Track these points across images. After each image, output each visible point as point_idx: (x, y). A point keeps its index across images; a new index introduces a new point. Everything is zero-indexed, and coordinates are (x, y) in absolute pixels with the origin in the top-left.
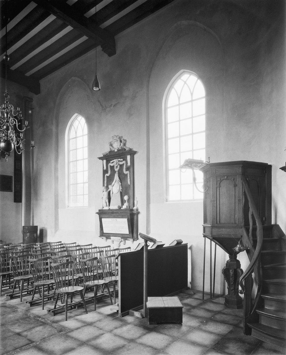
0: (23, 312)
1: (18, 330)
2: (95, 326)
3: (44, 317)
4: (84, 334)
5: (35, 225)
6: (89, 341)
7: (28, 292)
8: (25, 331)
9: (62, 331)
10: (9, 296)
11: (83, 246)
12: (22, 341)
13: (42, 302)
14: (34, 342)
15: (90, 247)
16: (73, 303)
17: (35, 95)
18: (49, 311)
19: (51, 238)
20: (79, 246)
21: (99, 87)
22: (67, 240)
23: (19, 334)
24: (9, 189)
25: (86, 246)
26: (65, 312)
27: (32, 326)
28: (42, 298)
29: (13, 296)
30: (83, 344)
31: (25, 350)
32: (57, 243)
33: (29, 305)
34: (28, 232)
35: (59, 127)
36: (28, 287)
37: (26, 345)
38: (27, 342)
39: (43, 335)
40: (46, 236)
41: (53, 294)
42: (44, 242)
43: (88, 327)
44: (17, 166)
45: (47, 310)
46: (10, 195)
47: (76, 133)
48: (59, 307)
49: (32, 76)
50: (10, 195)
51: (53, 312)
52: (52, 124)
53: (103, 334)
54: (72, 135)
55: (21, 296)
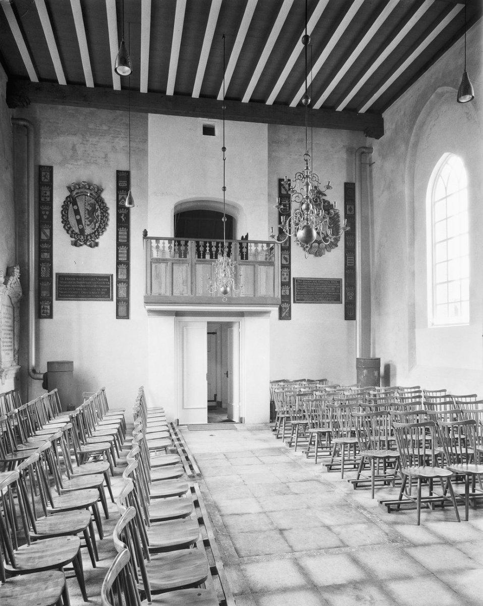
0: (342, 495)
1: (328, 521)
2: (460, 550)
3: (371, 510)
4: (433, 559)
5: (377, 357)
6: (441, 572)
7: (355, 465)
8: (338, 525)
9: (397, 542)
10: (326, 465)
11: (455, 397)
12: (332, 541)
13: (370, 486)
14: (348, 546)
15: (473, 399)
16: (433, 496)
17: (376, 141)
18: (381, 502)
19: (402, 380)
20: (449, 396)
21: (470, 94)
22: (430, 384)
23: (329, 528)
24: (337, 300)
25: (467, 401)
26: (416, 510)
27: (350, 520)
28: (372, 480)
29: (333, 467)
30: (430, 574)
31: (332, 554)
32: (411, 388)
33: (352, 486)
34: (365, 368)
35: (415, 183)
36: (355, 458)
37: (335, 547)
38: (338, 543)
39: (364, 540)
40: (395, 375)
41: (392, 475)
42: (392, 385)
43: (447, 547)
44: (352, 260)
45: (378, 501)
46: (339, 309)
47: (446, 188)
48: (407, 499)
49: (369, 111)
50: (339, 309)
51: (386, 505)
52: (404, 182)
53: (473, 569)
54: (440, 193)
55: (342, 469)
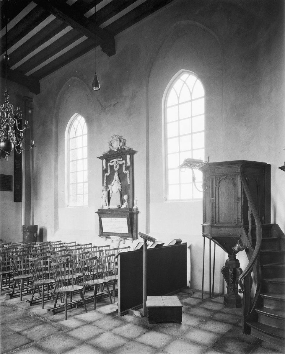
0: (23, 311)
1: (18, 329)
2: (95, 325)
3: (44, 316)
4: (84, 333)
5: (35, 224)
6: (88, 340)
7: (28, 291)
8: (25, 330)
9: (62, 330)
10: (9, 295)
11: (83, 245)
12: (22, 340)
13: (41, 301)
14: (34, 341)
15: (90, 246)
16: (72, 302)
17: (35, 95)
18: (49, 310)
19: (51, 237)
20: (78, 245)
21: (98, 87)
22: (67, 240)
23: (19, 333)
24: (9, 189)
25: (86, 246)
26: (65, 311)
27: (32, 325)
28: (42, 298)
29: (13, 295)
30: (82, 343)
31: (25, 349)
32: (56, 242)
33: (29, 304)
34: (28, 232)
35: (59, 127)
36: (28, 287)
37: (26, 344)
38: (27, 341)
39: (43, 334)
40: (46, 235)
41: (53, 293)
42: (44, 241)
43: (88, 326)
44: (17, 166)
45: (47, 310)
46: (10, 194)
47: (76, 132)
48: (59, 306)
49: (32, 76)
50: (10, 194)
51: (52, 311)
52: (52, 123)
53: (102, 333)
54: (72, 134)
55: (21, 295)
